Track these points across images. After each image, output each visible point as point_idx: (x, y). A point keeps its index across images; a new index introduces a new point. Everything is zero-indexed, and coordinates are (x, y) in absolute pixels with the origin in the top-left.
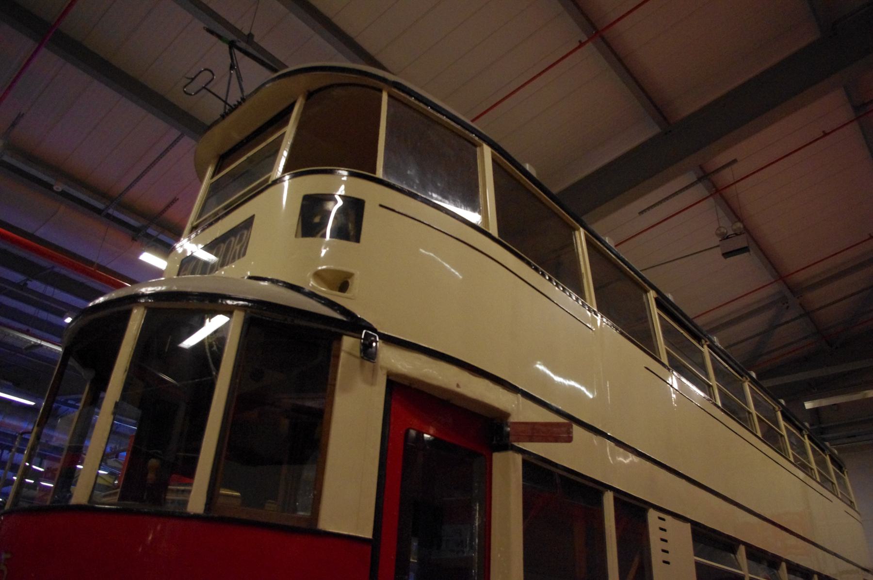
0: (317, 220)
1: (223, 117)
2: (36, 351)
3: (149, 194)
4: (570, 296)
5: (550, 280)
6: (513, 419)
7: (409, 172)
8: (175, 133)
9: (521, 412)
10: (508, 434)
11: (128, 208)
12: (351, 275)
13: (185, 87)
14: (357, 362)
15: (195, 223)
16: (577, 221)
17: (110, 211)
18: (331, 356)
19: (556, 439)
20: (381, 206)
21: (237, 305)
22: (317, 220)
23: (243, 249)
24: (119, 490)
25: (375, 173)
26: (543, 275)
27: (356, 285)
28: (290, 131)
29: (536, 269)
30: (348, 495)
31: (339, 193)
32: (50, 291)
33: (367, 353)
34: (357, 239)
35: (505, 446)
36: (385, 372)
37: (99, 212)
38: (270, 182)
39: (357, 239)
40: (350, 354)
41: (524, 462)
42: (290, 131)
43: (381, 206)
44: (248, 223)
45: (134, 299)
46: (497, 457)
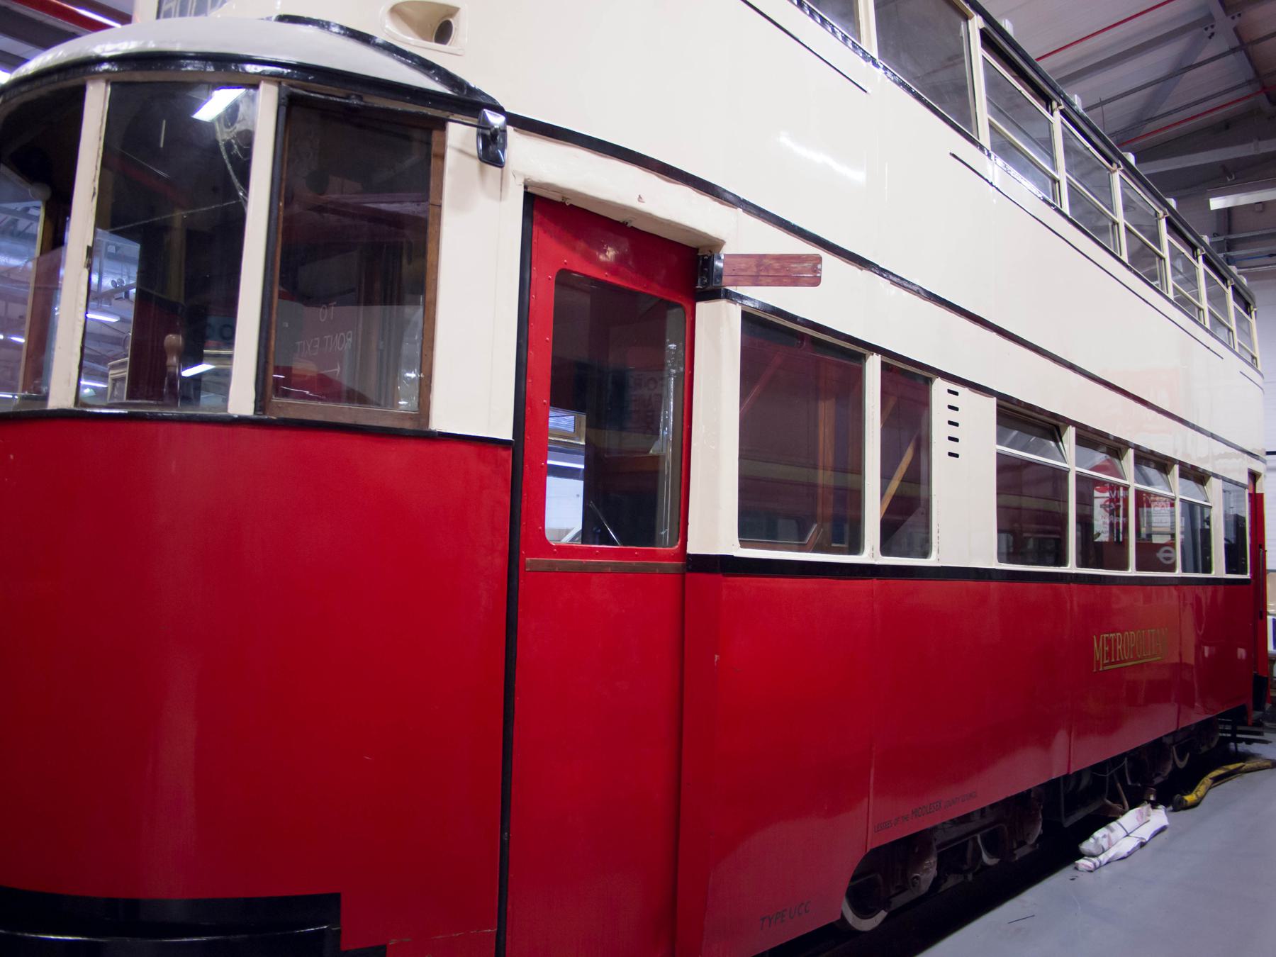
6: (726, 250)
9: (739, 236)
14: (476, 163)
19: (795, 281)
21: (262, 74)
24: (128, 359)
27: (461, 27)
30: (472, 372)
33: (491, 151)
35: (715, 294)
36: (521, 181)
40: (461, 151)
41: (745, 316)
45: (87, 66)
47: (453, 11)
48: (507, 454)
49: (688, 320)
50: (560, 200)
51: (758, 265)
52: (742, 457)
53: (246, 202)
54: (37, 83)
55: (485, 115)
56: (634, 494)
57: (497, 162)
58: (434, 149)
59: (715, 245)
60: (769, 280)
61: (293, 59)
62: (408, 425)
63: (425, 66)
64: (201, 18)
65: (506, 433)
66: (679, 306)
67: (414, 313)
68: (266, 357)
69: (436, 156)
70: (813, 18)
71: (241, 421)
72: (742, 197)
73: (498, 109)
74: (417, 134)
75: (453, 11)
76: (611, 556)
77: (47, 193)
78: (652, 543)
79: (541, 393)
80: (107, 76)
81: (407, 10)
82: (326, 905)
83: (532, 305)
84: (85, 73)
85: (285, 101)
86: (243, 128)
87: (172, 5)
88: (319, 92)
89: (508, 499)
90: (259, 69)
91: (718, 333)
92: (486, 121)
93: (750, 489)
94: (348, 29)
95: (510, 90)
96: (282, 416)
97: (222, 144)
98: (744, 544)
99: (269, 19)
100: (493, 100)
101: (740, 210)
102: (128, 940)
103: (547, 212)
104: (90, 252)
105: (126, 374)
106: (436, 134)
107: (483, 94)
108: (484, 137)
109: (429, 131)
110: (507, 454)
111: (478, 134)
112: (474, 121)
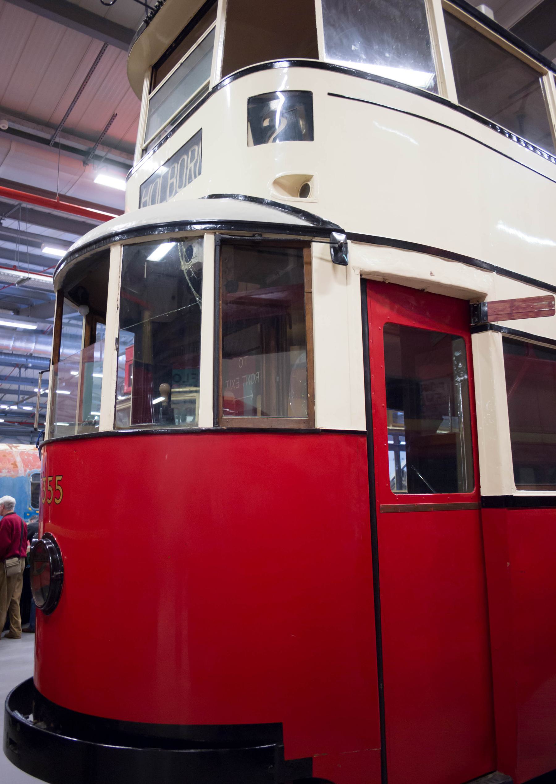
0: (266, 123)
1: (147, 23)
2: (25, 284)
3: (88, 116)
4: (542, 155)
5: (519, 141)
6: (488, 299)
7: (353, 48)
8: (98, 45)
9: (496, 290)
10: (486, 314)
11: (71, 132)
12: (309, 178)
13: (109, 5)
14: (330, 265)
15: (144, 146)
16: (545, 65)
17: (57, 140)
18: (302, 264)
19: (538, 314)
20: (330, 94)
21: (205, 229)
22: (266, 123)
23: (195, 163)
24: (131, 396)
25: (318, 58)
26: (510, 137)
27: (314, 186)
28: (220, 24)
29: (502, 132)
30: (338, 392)
31: (282, 88)
32: (23, 226)
33: (339, 256)
34: (311, 138)
35: (484, 327)
36: (358, 273)
37: (46, 142)
38: (210, 90)
39: (311, 138)
40: (322, 259)
41: (505, 339)
42: (220, 24)
43: (330, 94)
44: (197, 138)
45: (108, 238)
46: (476, 338)
47: (309, 178)
48: (363, 440)
49: (467, 345)
50: (382, 280)
51: (511, 307)
52: (512, 430)
53: (201, 303)
54: (85, 251)
55: (333, 236)
56: (444, 460)
57: (344, 262)
58: (305, 259)
59: (483, 296)
60: (519, 315)
61: (216, 219)
62: (303, 427)
63: (295, 211)
64: (164, 203)
65: (362, 427)
66: (459, 337)
67: (296, 357)
68: (218, 392)
69: (307, 263)
70: (528, 148)
71: (207, 432)
72: (495, 265)
73: (341, 231)
74: (291, 252)
75: (309, 178)
76: (427, 500)
77: (85, 310)
78: (456, 491)
79: (381, 402)
80: (121, 242)
81: (283, 181)
82: (273, 731)
83: (371, 346)
84: (109, 242)
85: (219, 243)
86: (196, 261)
87: (147, 198)
88: (238, 234)
89: (366, 468)
90: (203, 226)
91: (488, 353)
92: (334, 239)
93: (519, 450)
94: (249, 197)
95: (345, 217)
96: (229, 426)
97: (185, 272)
98: (519, 488)
99: (203, 198)
100: (337, 226)
101: (494, 273)
102: (160, 750)
103: (374, 287)
104: (117, 340)
105: (131, 405)
106: (305, 251)
107: (332, 223)
108: (334, 248)
109: (300, 249)
110: (363, 440)
111: (331, 247)
112: (328, 240)
